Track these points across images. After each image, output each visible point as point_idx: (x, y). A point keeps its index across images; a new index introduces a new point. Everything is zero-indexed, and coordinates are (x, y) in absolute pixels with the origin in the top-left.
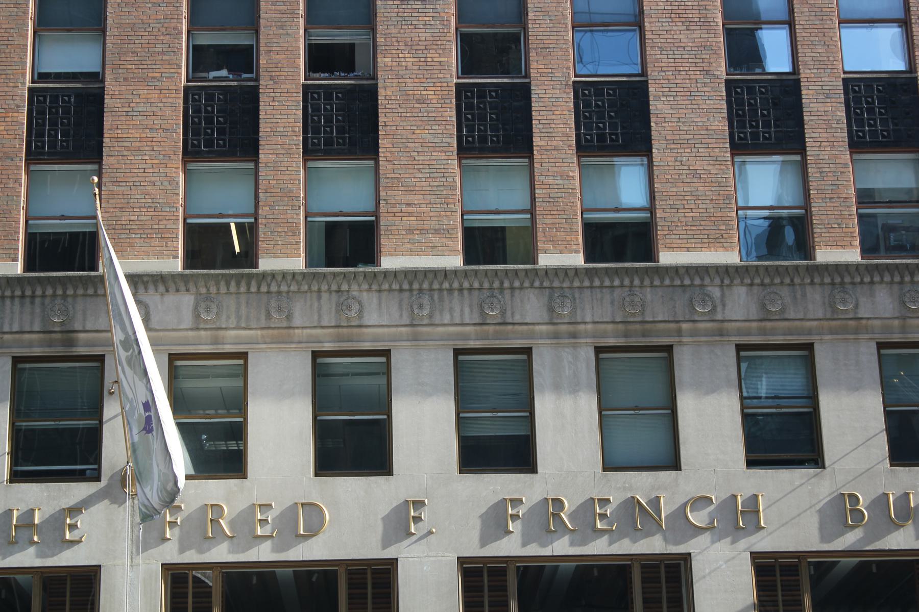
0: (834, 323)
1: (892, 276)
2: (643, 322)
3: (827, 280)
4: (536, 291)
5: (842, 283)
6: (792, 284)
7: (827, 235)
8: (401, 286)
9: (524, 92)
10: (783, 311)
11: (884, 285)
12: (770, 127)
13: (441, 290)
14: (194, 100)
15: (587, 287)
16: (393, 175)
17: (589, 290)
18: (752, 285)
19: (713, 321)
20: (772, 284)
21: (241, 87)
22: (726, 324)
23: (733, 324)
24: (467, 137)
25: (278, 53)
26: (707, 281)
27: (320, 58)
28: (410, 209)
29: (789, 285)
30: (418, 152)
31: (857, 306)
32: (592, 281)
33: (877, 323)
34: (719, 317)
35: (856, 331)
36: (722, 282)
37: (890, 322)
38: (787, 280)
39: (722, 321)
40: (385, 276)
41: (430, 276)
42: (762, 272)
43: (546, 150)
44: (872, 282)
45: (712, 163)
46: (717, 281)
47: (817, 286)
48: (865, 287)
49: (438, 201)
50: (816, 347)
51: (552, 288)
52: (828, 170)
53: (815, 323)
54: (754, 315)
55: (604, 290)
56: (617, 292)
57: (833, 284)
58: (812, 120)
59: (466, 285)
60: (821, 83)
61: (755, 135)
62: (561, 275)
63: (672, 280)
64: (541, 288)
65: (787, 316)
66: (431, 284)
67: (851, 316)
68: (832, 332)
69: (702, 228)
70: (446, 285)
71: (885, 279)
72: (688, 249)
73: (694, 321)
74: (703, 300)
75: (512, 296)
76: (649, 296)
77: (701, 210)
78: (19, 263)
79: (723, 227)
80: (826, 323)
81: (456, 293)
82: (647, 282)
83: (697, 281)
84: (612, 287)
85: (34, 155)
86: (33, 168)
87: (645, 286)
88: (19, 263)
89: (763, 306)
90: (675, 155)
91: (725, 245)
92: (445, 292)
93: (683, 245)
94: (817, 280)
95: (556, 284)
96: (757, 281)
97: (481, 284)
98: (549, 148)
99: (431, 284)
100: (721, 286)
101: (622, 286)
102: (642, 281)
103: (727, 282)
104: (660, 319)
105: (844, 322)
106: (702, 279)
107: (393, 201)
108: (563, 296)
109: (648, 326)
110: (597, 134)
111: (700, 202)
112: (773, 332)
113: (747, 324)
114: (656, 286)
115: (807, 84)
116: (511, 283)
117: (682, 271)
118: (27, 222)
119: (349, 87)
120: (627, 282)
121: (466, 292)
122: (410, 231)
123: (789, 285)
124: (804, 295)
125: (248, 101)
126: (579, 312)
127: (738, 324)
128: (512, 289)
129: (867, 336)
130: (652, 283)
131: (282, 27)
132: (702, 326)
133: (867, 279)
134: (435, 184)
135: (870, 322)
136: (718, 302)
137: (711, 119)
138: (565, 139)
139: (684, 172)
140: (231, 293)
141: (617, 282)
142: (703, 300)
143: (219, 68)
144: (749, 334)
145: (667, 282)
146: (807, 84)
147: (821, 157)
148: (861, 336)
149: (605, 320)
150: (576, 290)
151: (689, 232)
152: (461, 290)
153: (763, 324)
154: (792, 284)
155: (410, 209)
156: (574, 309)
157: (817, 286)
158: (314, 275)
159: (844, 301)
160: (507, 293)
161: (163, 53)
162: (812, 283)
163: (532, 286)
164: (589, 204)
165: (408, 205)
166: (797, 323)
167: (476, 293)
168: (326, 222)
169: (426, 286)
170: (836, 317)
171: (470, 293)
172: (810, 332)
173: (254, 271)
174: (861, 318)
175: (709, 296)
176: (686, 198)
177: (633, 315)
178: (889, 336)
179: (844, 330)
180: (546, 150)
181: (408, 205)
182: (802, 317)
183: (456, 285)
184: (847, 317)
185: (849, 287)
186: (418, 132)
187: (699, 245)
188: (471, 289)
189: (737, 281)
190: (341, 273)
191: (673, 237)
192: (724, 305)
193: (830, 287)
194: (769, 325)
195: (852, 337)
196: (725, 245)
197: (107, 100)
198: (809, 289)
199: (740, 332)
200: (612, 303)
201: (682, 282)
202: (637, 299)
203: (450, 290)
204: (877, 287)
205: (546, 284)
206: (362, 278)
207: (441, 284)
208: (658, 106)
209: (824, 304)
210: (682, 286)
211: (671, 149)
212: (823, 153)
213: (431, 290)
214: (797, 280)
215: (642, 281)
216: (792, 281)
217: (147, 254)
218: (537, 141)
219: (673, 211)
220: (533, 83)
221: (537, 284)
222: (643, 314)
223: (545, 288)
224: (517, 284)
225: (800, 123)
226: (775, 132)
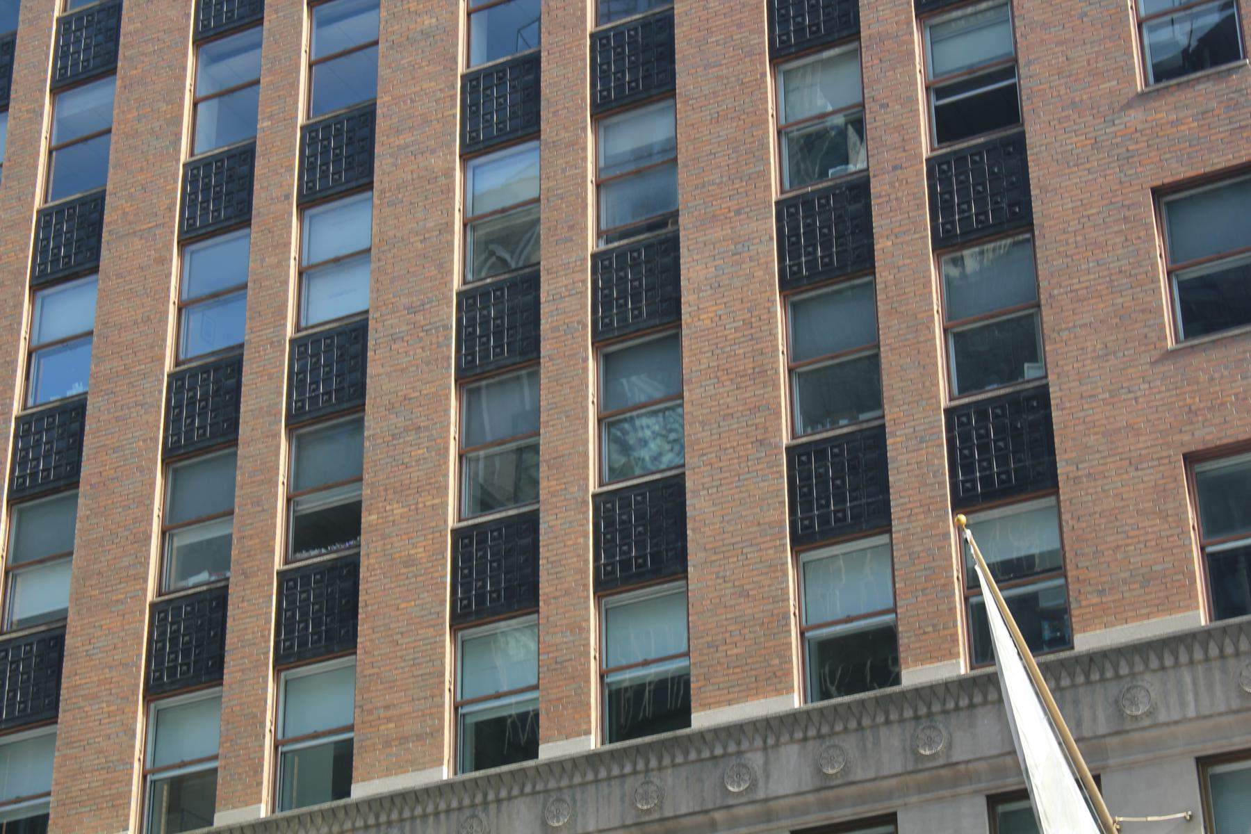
0: (920, 776)
1: (1161, 658)
2: (662, 820)
3: (908, 713)
4: (528, 800)
5: (930, 715)
6: (860, 728)
7: (918, 645)
8: (365, 822)
9: (876, 439)
10: (846, 771)
11: (989, 707)
12: (845, 501)
13: (413, 818)
14: (961, 424)
15: (592, 782)
16: (371, 671)
17: (594, 786)
18: (805, 739)
19: (754, 802)
20: (833, 734)
21: (861, 431)
22: (771, 804)
23: (782, 802)
24: (963, 482)
25: (251, 537)
26: (745, 745)
27: (308, 531)
28: (389, 713)
29: (857, 730)
30: (402, 634)
31: (950, 746)
32: (596, 773)
33: (981, 765)
34: (761, 795)
35: (956, 782)
36: (765, 742)
37: (1000, 760)
38: (853, 724)
39: (767, 800)
40: (346, 812)
41: (398, 801)
42: (815, 718)
43: (555, 598)
44: (972, 706)
45: (764, 570)
46: (758, 743)
47: (895, 726)
48: (963, 714)
49: (422, 695)
50: (900, 817)
51: (547, 791)
52: (919, 548)
53: (893, 782)
54: (808, 783)
55: (613, 782)
56: (629, 781)
57: (917, 718)
58: (900, 480)
59: (442, 806)
60: (912, 424)
61: (824, 519)
62: (557, 770)
63: (699, 752)
64: (534, 793)
65: (852, 778)
66: (401, 813)
67: (942, 761)
68: (921, 789)
69: (747, 668)
70: (419, 811)
71: (990, 698)
72: (730, 703)
73: (728, 807)
74: (739, 774)
75: (499, 810)
76: (670, 781)
77: (749, 642)
78: (962, 661)
79: (776, 661)
80: (908, 778)
81: (431, 819)
82: (666, 761)
83: (732, 748)
84: (623, 776)
85: (802, 540)
86: (805, 557)
87: (666, 767)
88: (962, 661)
89: (819, 771)
90: (716, 569)
91: (778, 686)
92: (418, 821)
93: (723, 698)
94: (894, 716)
95: (552, 784)
96: (812, 732)
97: (460, 802)
98: (558, 594)
99: (401, 813)
100: (765, 748)
101: (635, 772)
102: (660, 761)
103: (771, 741)
104: (683, 810)
105: (934, 772)
106: (739, 743)
107: (369, 706)
108: (559, 800)
109: (670, 824)
110: (620, 562)
111: (746, 631)
112: (839, 803)
113: (801, 799)
114: (679, 765)
115: (893, 428)
116: (497, 794)
117: (709, 737)
118: (802, 634)
119: (329, 564)
120: (641, 765)
121: (443, 816)
122: (387, 743)
123: (857, 730)
124: (877, 743)
125: (872, 447)
126: (580, 819)
127: (787, 801)
128: (499, 801)
129: (968, 788)
130: (673, 761)
131: (258, 503)
132: (740, 811)
133: (964, 702)
134: (420, 672)
135: (970, 766)
136: (760, 773)
137: (765, 508)
138: (578, 577)
139: (727, 591)
140: (539, 793)
141: (628, 769)
142: (739, 774)
143: (198, 572)
144: (805, 810)
145: (693, 756)
146: (893, 428)
147: (912, 531)
148: (960, 790)
149: (613, 825)
150: (578, 789)
151: (731, 677)
152: (437, 814)
153: (823, 794)
154: (860, 728)
155: (389, 713)
156: (573, 818)
157: (895, 726)
158: (1224, 630)
159: (930, 743)
160: (493, 807)
161: (128, 568)
162: (888, 722)
163: (522, 794)
164: (618, 659)
165: (387, 707)
166: (868, 785)
167: (454, 815)
168: (336, 743)
169: (394, 816)
170: (920, 767)
171: (448, 818)
172: (890, 795)
173: (896, 689)
174: (957, 763)
175: (745, 766)
176: (729, 628)
177: (648, 812)
178: (1000, 783)
179: (938, 784)
180: (555, 598)
181: (387, 707)
182: (873, 775)
183: (430, 809)
184: (936, 763)
185: (939, 718)
186: (403, 606)
187: (744, 694)
188: (448, 811)
189: (785, 738)
190: (294, 817)
191: (711, 688)
192: (767, 777)
193: (913, 723)
194: (830, 794)
195: (947, 793)
196: (778, 686)
197: (69, 641)
198: (883, 731)
199: (794, 812)
200: (622, 800)
201: (712, 752)
202: (653, 788)
203: (425, 816)
204: (980, 711)
205: (539, 787)
206: (367, 809)
207: (412, 810)
208: (696, 505)
209: (904, 749)
210: (713, 758)
211: (712, 562)
212: (914, 524)
213: (402, 820)
214: (866, 722)
215: (660, 761)
216: (859, 723)
217: (719, 704)
218: (545, 588)
219: (712, 650)
220: (542, 508)
221: (528, 789)
222: (661, 808)
223: (539, 793)
224: (503, 794)
225: (884, 486)
226: (851, 508)
